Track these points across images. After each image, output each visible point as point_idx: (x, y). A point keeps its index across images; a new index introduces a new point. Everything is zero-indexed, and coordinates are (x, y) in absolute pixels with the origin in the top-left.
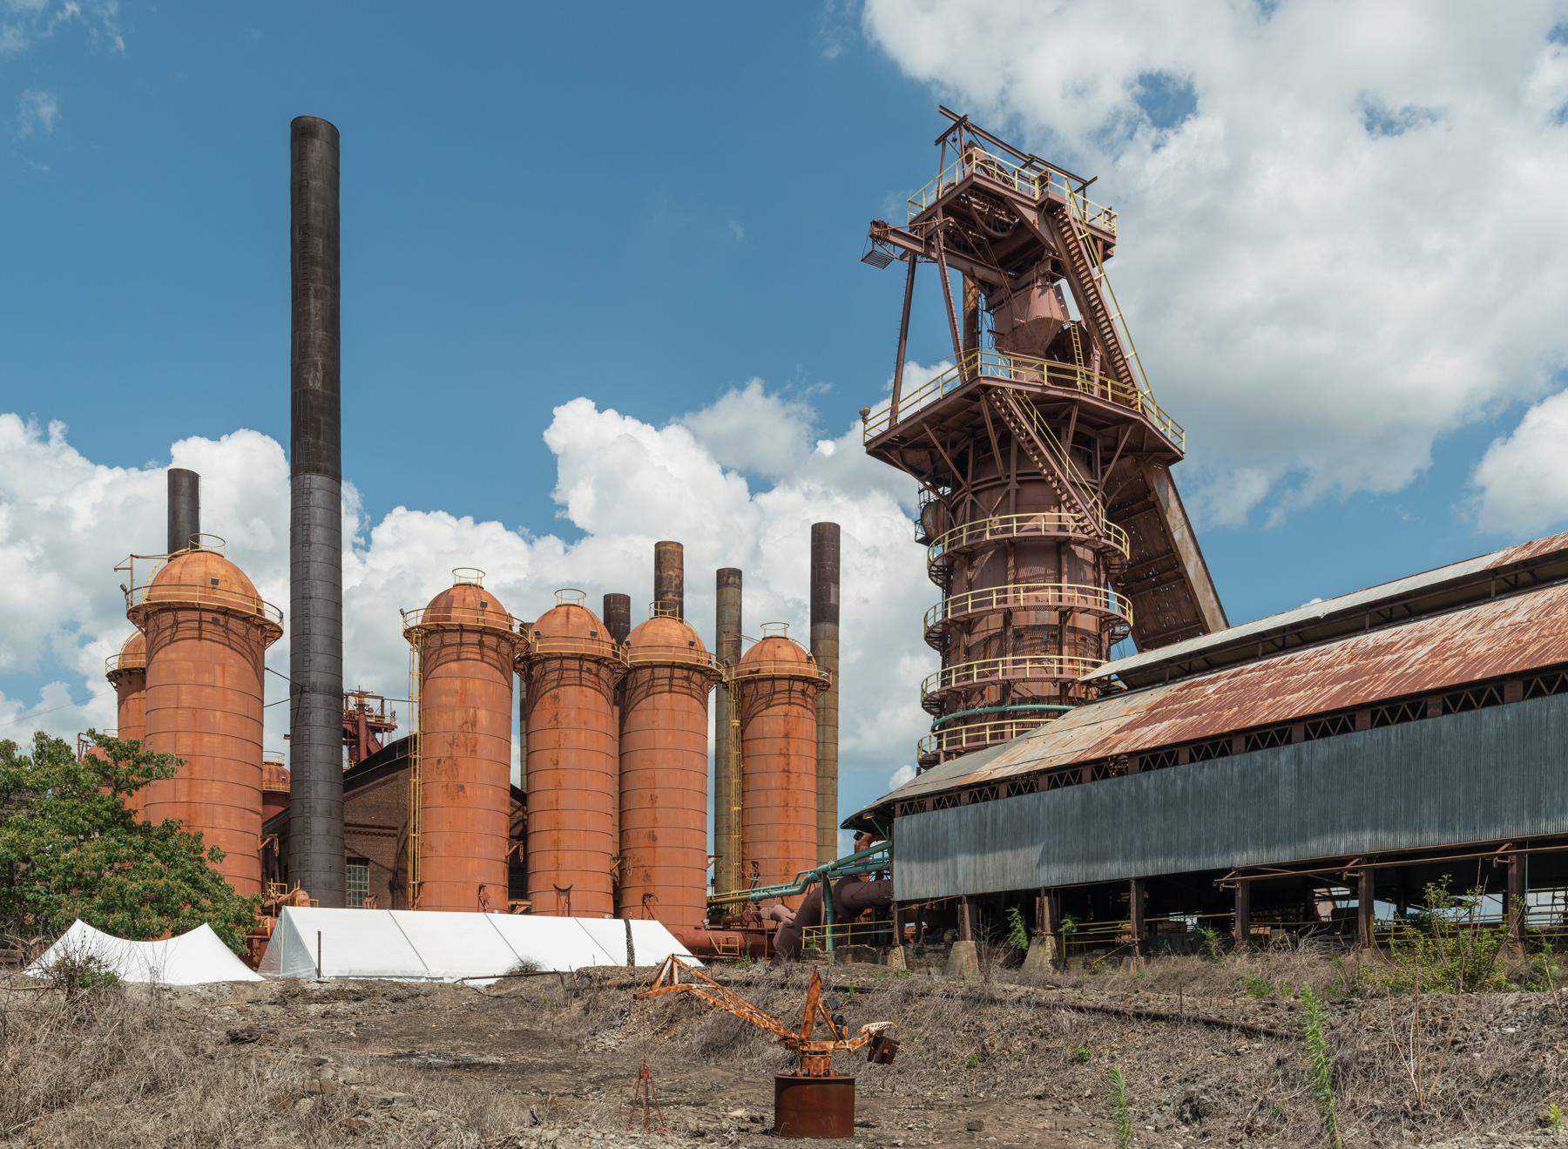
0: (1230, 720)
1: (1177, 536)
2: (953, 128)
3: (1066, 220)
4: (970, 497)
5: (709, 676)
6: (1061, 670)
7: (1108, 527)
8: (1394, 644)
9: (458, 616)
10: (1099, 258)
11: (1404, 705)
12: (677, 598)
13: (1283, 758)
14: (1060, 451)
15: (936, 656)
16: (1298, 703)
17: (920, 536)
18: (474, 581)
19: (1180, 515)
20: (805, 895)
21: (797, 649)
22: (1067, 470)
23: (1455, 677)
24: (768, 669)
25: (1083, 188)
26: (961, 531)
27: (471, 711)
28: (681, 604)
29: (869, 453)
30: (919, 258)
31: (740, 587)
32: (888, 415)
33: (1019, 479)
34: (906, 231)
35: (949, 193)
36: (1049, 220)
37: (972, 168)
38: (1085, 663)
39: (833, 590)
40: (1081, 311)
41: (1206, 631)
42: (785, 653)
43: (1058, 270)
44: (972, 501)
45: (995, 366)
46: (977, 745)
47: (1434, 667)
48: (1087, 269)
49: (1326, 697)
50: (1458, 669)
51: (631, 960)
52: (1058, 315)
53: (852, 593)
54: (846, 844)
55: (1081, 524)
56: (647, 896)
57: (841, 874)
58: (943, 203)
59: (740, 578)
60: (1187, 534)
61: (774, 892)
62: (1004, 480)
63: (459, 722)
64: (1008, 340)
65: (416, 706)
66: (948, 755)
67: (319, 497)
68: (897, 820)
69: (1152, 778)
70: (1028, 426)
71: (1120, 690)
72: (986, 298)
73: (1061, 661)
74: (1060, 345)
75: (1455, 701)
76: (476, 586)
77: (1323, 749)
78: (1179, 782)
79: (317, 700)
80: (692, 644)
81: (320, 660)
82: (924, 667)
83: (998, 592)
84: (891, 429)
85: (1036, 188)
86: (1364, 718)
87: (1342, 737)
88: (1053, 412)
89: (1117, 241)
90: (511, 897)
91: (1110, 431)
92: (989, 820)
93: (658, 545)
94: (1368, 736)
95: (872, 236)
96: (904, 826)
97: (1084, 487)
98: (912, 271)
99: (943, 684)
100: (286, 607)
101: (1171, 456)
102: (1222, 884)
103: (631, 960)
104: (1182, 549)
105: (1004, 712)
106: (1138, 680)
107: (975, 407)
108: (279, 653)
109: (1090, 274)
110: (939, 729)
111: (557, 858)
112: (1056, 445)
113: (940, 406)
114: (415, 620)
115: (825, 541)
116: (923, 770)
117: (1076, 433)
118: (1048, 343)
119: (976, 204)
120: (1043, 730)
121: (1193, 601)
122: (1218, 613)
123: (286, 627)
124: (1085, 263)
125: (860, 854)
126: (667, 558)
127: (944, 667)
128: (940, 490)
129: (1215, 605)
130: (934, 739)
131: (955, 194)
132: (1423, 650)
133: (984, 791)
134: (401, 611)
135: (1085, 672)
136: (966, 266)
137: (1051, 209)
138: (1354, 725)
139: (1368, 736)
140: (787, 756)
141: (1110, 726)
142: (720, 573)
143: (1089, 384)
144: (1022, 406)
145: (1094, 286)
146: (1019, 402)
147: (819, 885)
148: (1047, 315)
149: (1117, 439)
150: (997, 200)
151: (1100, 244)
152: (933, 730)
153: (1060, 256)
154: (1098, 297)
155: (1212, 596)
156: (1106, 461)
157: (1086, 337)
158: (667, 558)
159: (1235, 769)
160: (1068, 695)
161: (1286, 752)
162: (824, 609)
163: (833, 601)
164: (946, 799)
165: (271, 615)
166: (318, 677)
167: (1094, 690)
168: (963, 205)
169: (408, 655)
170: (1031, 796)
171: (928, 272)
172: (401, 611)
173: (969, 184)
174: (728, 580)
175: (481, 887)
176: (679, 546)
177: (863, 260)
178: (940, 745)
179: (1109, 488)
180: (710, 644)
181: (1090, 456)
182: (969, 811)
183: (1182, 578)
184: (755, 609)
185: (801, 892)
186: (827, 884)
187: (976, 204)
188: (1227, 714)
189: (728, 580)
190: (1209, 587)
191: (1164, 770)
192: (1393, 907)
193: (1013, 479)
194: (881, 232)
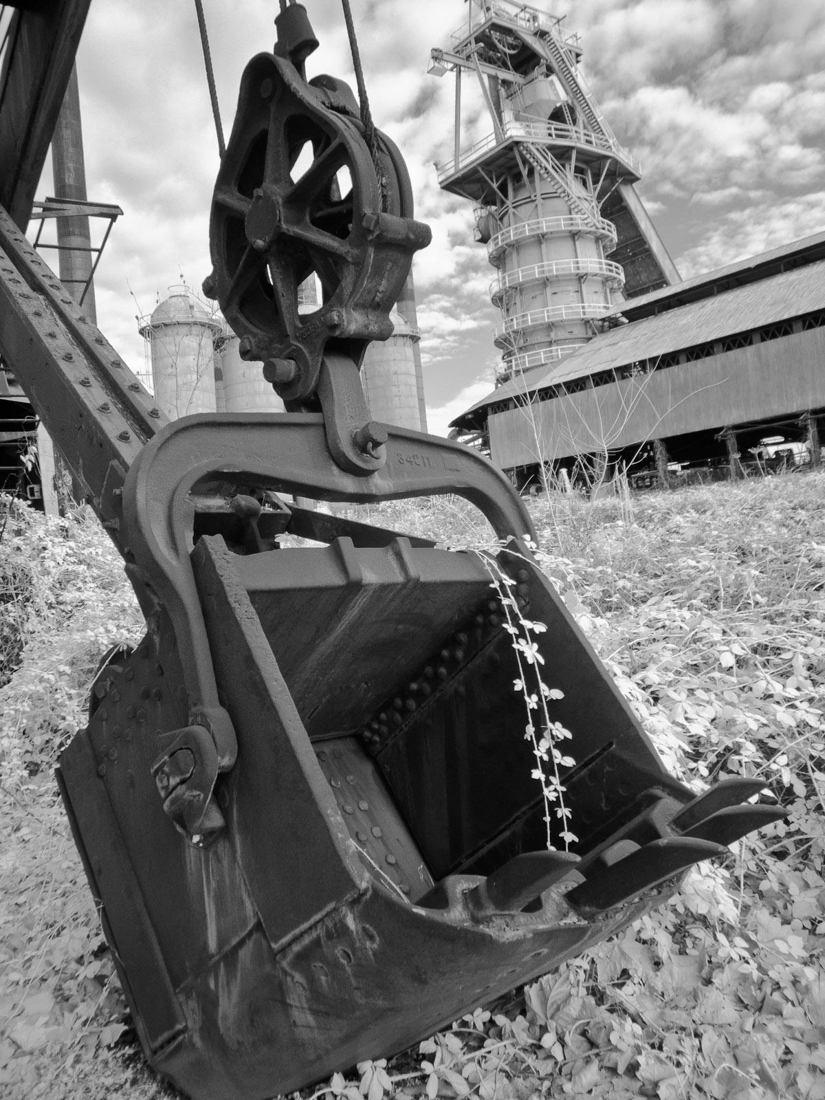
3: (552, 41)
6: (584, 313)
10: (574, 61)
11: (573, 384)
13: (749, 354)
17: (478, 238)
18: (183, 293)
26: (497, 237)
29: (443, 188)
30: (462, 69)
33: (543, 196)
34: (452, 53)
40: (567, 94)
41: (668, 284)
43: (550, 70)
44: (514, 213)
45: (515, 131)
48: (568, 69)
52: (553, 98)
55: (586, 222)
58: (475, 35)
62: (533, 198)
65: (151, 377)
68: (490, 418)
70: (548, 162)
72: (506, 91)
73: (583, 307)
75: (692, 354)
76: (185, 296)
78: (681, 375)
86: (683, 358)
88: (561, 154)
91: (595, 164)
95: (433, 57)
98: (76, 281)
101: (632, 178)
102: (719, 437)
107: (510, 155)
109: (570, 72)
114: (146, 322)
116: (499, 385)
117: (576, 167)
119: (495, 36)
121: (656, 265)
124: (566, 66)
131: (482, 30)
134: (137, 318)
138: (792, 330)
143: (577, 137)
144: (540, 152)
145: (573, 79)
146: (538, 149)
149: (599, 169)
150: (507, 31)
151: (573, 54)
154: (577, 86)
156: (595, 182)
159: (718, 364)
167: (606, 324)
168: (487, 36)
169: (143, 344)
170: (582, 392)
173: (490, 23)
177: (428, 72)
183: (648, 253)
187: (495, 36)
191: (671, 368)
193: (539, 197)
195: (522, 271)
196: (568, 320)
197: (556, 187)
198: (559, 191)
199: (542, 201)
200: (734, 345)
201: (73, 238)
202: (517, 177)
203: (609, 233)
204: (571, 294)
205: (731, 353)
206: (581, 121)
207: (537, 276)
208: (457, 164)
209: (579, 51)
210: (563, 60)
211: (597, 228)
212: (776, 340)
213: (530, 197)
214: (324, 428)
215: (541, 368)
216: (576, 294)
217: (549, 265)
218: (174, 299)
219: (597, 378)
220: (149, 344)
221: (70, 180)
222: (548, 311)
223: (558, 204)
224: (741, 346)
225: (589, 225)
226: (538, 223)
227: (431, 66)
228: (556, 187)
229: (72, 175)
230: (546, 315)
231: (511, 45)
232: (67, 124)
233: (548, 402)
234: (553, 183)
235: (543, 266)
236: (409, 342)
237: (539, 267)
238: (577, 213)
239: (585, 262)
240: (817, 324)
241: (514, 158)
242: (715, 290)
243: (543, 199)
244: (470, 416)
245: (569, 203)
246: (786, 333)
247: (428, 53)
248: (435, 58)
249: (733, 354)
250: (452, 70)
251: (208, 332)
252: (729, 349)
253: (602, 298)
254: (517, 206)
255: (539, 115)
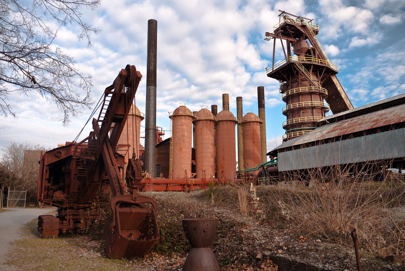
0: (349, 131)
1: (339, 89)
2: (282, 13)
4: (290, 84)
5: (236, 122)
7: (322, 89)
8: (386, 113)
9: (181, 113)
12: (228, 106)
14: (310, 75)
15: (286, 117)
16: (365, 127)
17: (280, 92)
18: (184, 105)
19: (339, 84)
20: (259, 170)
21: (255, 116)
22: (312, 77)
23: (397, 122)
24: (249, 120)
25: (311, 21)
26: (289, 91)
27: (183, 132)
28: (229, 106)
29: (268, 76)
31: (242, 101)
32: (272, 68)
35: (282, 25)
36: (304, 28)
37: (236, 185)
38: (319, 118)
39: (263, 101)
40: (312, 45)
41: (348, 109)
42: (253, 116)
43: (306, 38)
45: (295, 58)
46: (295, 137)
47: (393, 119)
49: (370, 126)
50: (398, 119)
51: (143, 138)
52: (307, 47)
53: (268, 102)
54: (268, 159)
56: (222, 171)
57: (267, 165)
59: (242, 99)
60: (341, 88)
61: (252, 170)
63: (181, 135)
64: (297, 52)
65: (172, 132)
66: (289, 139)
67: (152, 90)
69: (334, 144)
70: (303, 69)
71: (328, 123)
74: (308, 52)
77: (371, 137)
79: (151, 131)
80: (231, 116)
81: (152, 124)
82: (284, 120)
83: (298, 104)
84: (273, 71)
85: (300, 23)
87: (374, 134)
88: (308, 67)
89: (319, 31)
90: (192, 172)
92: (299, 154)
93: (223, 95)
94: (380, 134)
96: (279, 154)
97: (315, 81)
99: (287, 123)
100: (144, 112)
103: (143, 138)
104: (340, 92)
105: (301, 129)
106: (332, 121)
108: (143, 123)
110: (287, 133)
111: (202, 163)
112: (309, 74)
113: (282, 67)
114: (172, 114)
115: (261, 91)
116: (284, 142)
118: (306, 52)
120: (310, 133)
122: (350, 105)
123: (145, 117)
125: (272, 160)
126: (225, 98)
127: (287, 120)
128: (284, 82)
129: (349, 103)
130: (286, 135)
132: (392, 115)
133: (297, 147)
134: (169, 112)
135: (319, 120)
136: (287, 39)
137: (304, 26)
139: (380, 134)
140: (254, 139)
141: (324, 132)
142: (237, 98)
143: (315, 61)
147: (262, 168)
148: (305, 47)
152: (286, 133)
153: (307, 35)
155: (348, 101)
156: (320, 75)
157: (314, 50)
158: (225, 98)
160: (317, 125)
161: (363, 138)
162: (261, 104)
163: (263, 103)
164: (289, 149)
165: (142, 115)
166: (151, 127)
169: (170, 122)
171: (278, 40)
172: (169, 112)
173: (286, 24)
174: (239, 100)
175: (186, 171)
176: (228, 94)
178: (287, 137)
179: (322, 80)
180: (235, 116)
181: (316, 74)
182: (294, 151)
184: (245, 103)
185: (258, 170)
186: (264, 168)
188: (350, 129)
189: (239, 100)
190: (348, 99)
192: (398, 170)
193: (300, 80)
194: (268, 34)
195: (293, 105)
196: (307, 122)
197: (305, 77)
198: (306, 79)
199: (301, 82)
200: (385, 130)
201: (151, 86)
202: (293, 74)
203: (324, 93)
204: (309, 113)
205: (356, 138)
206: (317, 54)
207: (297, 107)
208: (273, 68)
209: (317, 31)
210: (311, 34)
211: (320, 91)
212: (371, 135)
213: (297, 80)
214: (132, 196)
215: (297, 138)
216: (311, 113)
217: (302, 103)
218: (181, 107)
219: (295, 147)
220: (172, 121)
221: (152, 68)
222: (300, 119)
223: (305, 83)
224: (360, 136)
225: (317, 90)
226: (299, 89)
227: (265, 38)
228: (305, 77)
229: (153, 67)
230: (300, 120)
231: (293, 29)
232: (152, 51)
233: (297, 150)
234: (304, 76)
235: (300, 103)
236: (258, 124)
237: (298, 104)
238: (312, 86)
239: (315, 102)
240: (385, 130)
241: (291, 68)
242: (380, 108)
243: (301, 81)
244: (272, 153)
245: (310, 82)
246: (375, 133)
247: (265, 34)
248: (266, 35)
249: (307, 149)
250: (273, 38)
251: (191, 118)
252: (356, 137)
253: (321, 115)
254: (293, 83)
255: (302, 53)
